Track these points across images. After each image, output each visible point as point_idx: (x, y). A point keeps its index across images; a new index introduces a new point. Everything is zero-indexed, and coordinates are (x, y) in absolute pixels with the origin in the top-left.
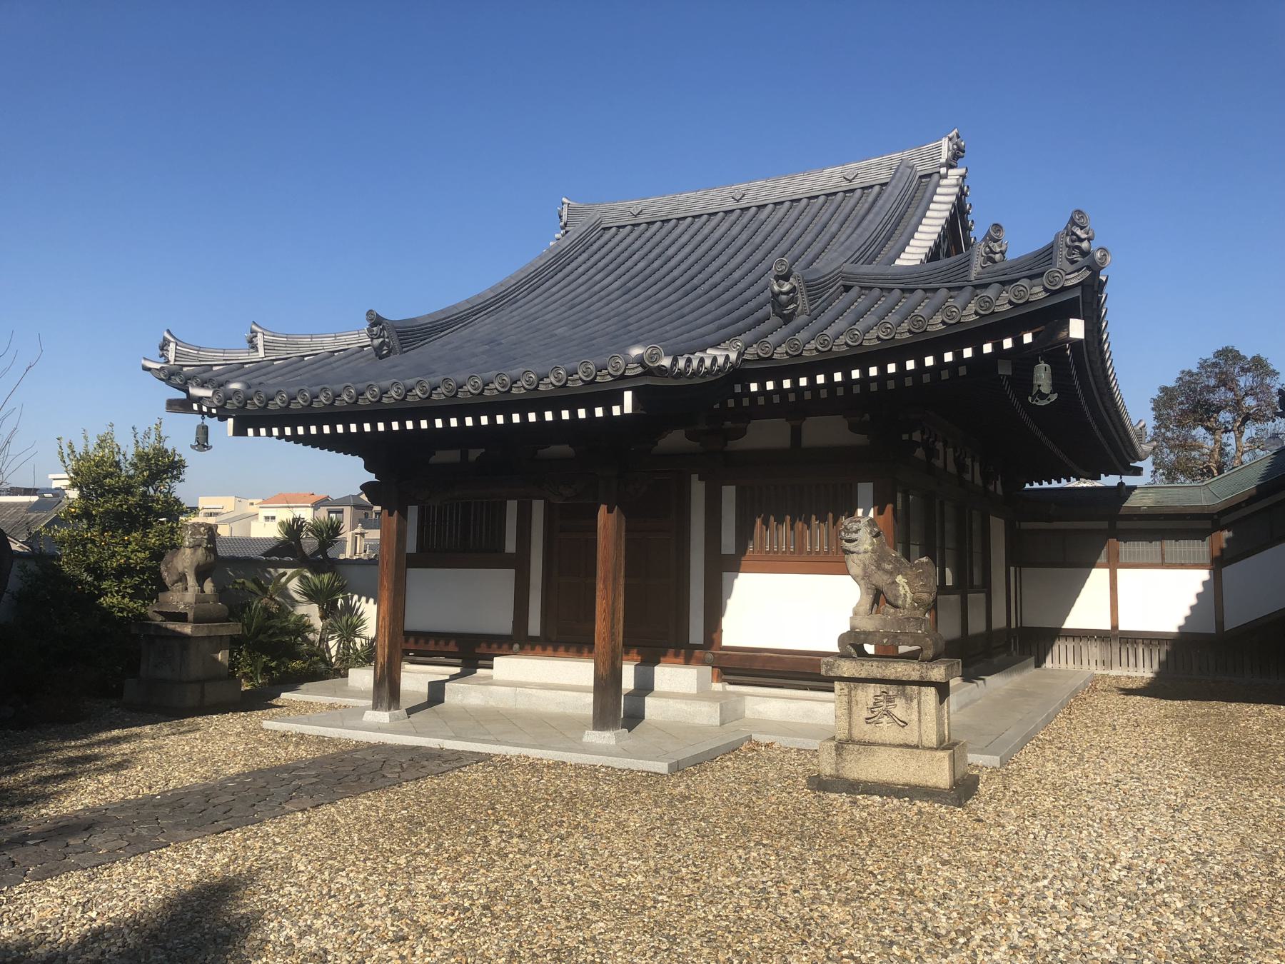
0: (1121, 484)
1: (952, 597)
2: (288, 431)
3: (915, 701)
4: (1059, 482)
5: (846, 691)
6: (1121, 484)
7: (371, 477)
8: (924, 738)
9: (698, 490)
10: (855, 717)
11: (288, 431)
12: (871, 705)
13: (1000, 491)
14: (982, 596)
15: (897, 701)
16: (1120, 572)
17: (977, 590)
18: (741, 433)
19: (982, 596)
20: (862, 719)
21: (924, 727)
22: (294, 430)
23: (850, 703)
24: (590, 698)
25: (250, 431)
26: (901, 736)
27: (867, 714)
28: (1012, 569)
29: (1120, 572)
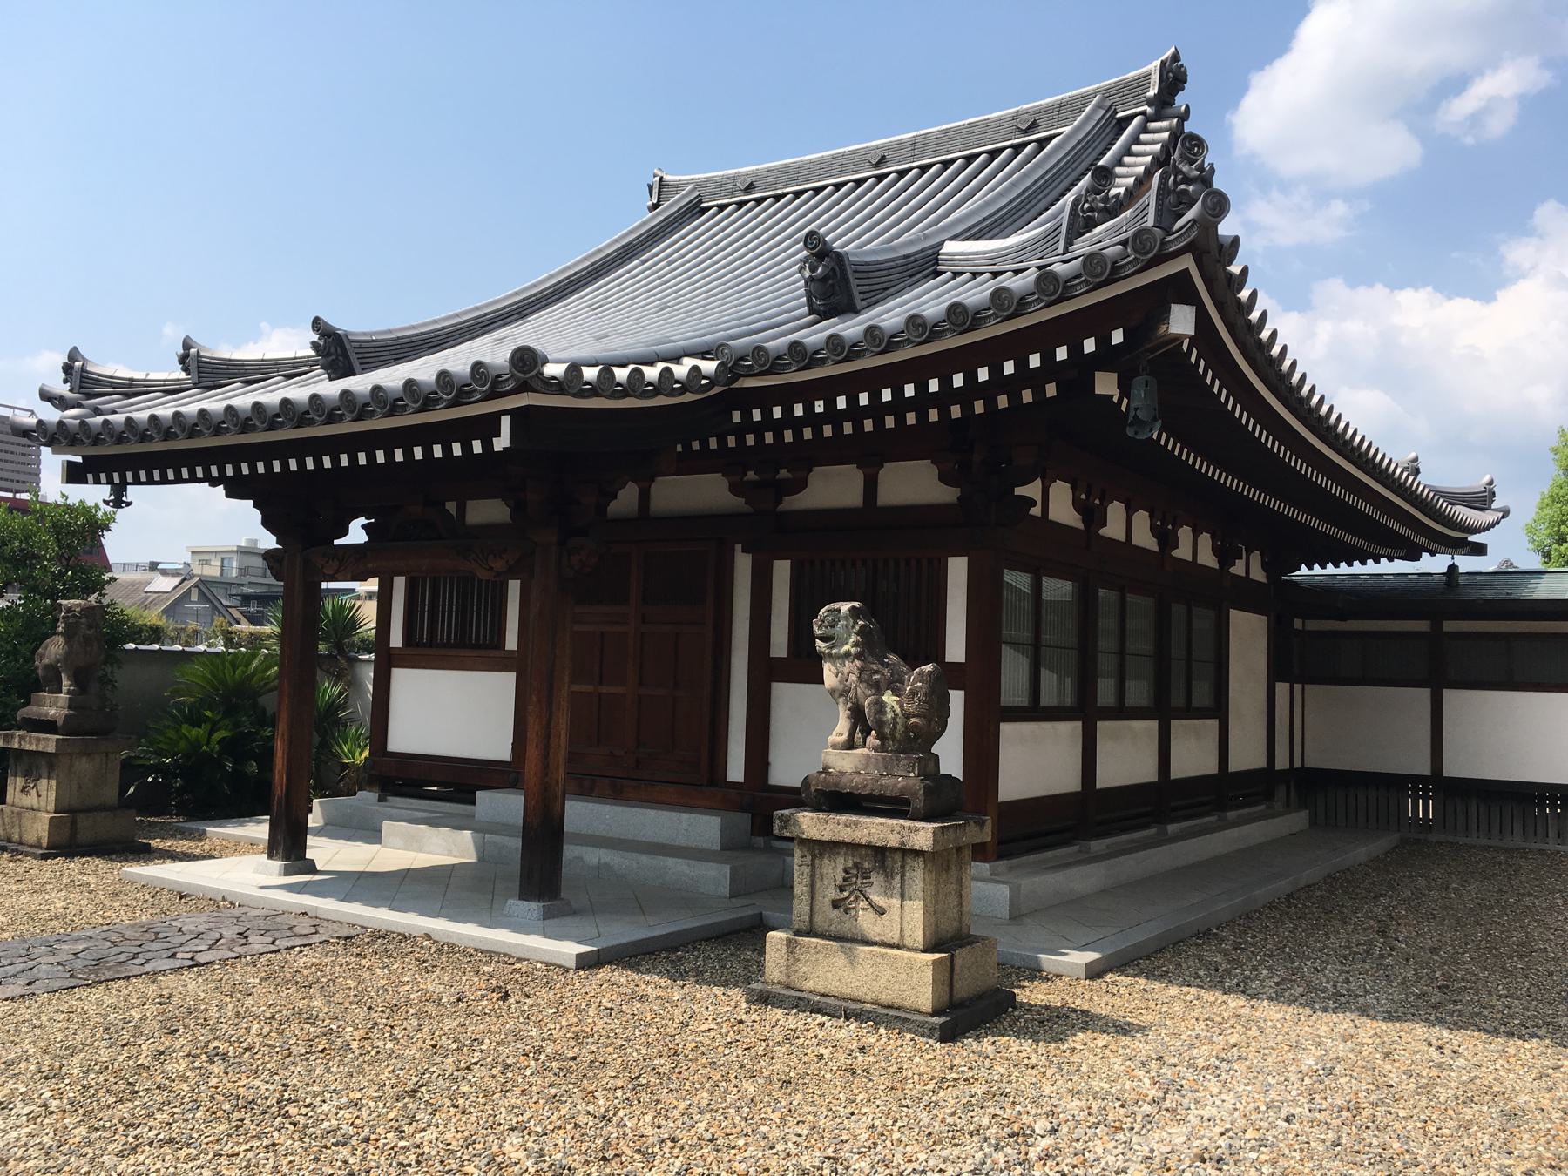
0: (1453, 568)
1: (1138, 725)
2: (214, 472)
3: (898, 879)
4: (1310, 568)
5: (809, 858)
6: (1453, 568)
7: (269, 541)
8: (907, 934)
9: (743, 564)
10: (818, 898)
11: (214, 472)
12: (839, 881)
13: (1258, 575)
14: (1213, 724)
15: (874, 877)
16: (1449, 696)
17: (1190, 712)
18: (800, 485)
19: (1213, 724)
20: (827, 901)
21: (907, 918)
22: (222, 470)
23: (813, 876)
24: (516, 843)
25: (90, 477)
26: (878, 929)
27: (832, 894)
28: (1282, 689)
29: (1449, 696)
